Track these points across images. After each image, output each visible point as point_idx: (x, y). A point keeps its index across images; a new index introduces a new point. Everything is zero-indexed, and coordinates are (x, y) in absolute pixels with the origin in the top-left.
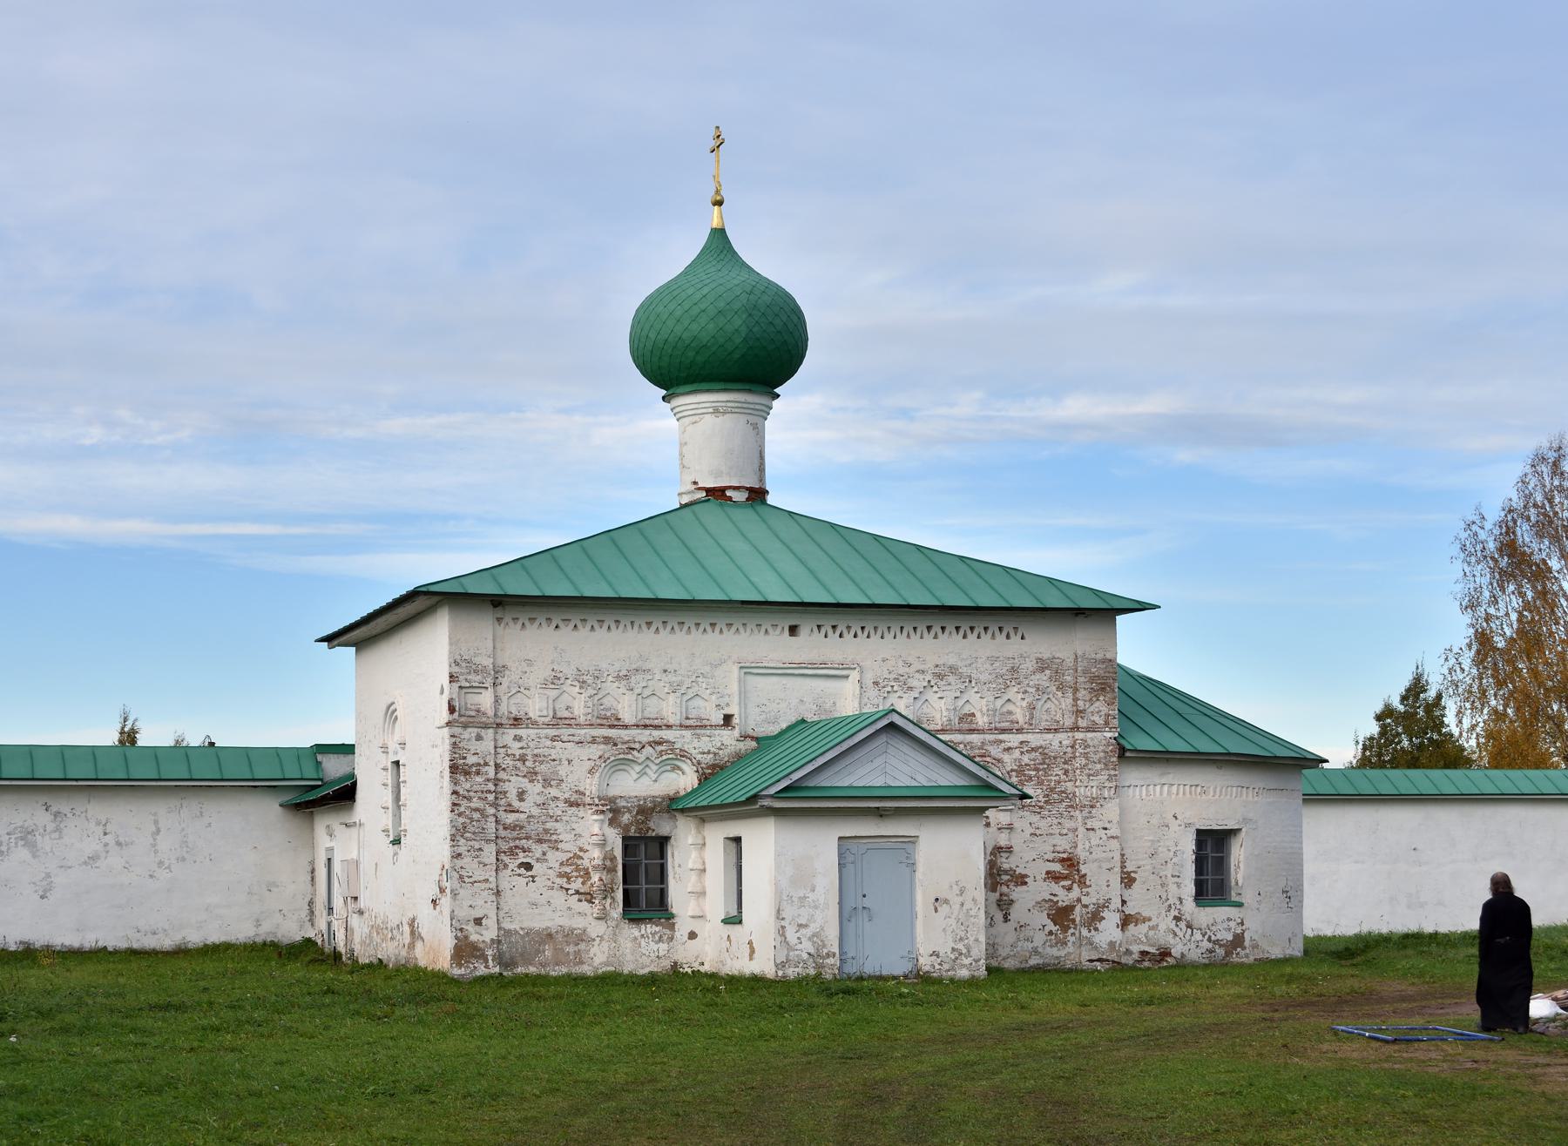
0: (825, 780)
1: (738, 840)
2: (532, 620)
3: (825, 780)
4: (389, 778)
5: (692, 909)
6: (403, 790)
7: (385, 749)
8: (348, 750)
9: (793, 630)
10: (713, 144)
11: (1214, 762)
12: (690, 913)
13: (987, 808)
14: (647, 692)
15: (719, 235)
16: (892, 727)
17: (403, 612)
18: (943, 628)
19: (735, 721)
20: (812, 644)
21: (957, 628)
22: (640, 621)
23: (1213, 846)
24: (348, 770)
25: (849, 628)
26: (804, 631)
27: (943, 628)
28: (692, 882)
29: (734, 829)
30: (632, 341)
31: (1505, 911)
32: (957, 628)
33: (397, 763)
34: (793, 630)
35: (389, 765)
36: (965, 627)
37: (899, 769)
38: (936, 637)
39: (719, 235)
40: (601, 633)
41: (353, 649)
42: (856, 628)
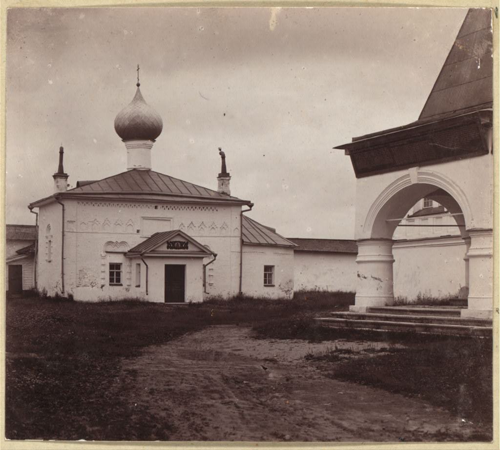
0: (157, 250)
7: (47, 237)
9: (156, 207)
11: (447, 238)
14: (117, 224)
16: (179, 235)
18: (196, 208)
19: (140, 232)
21: (200, 208)
22: (116, 204)
23: (268, 269)
25: (171, 207)
26: (159, 207)
27: (196, 208)
28: (128, 276)
31: (469, 244)
32: (200, 208)
33: (50, 241)
34: (156, 207)
35: (48, 241)
36: (202, 207)
38: (194, 210)
40: (105, 207)
41: (38, 208)
42: (186, 207)
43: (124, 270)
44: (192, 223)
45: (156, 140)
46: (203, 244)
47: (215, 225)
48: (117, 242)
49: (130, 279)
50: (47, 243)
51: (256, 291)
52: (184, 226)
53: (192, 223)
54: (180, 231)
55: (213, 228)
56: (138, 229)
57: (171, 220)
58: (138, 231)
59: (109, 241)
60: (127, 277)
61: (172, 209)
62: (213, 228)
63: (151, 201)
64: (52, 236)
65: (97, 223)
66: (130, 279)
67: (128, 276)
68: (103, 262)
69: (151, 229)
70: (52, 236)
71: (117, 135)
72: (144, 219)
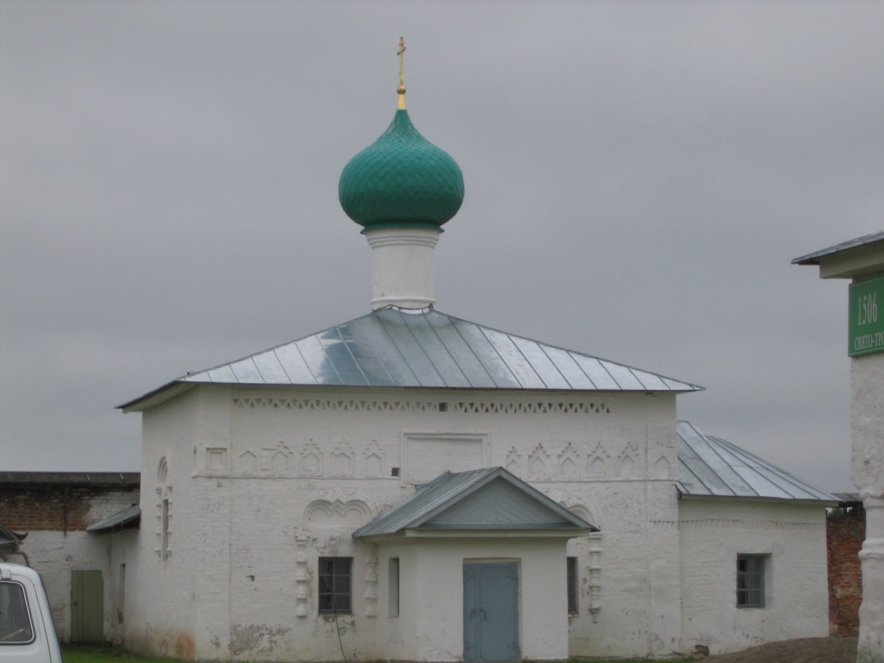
1: (397, 560)
2: (259, 400)
3: (455, 520)
4: (160, 513)
5: (368, 610)
6: (170, 522)
7: (159, 491)
8: (129, 485)
10: (399, 49)
12: (367, 613)
13: (568, 538)
15: (402, 117)
17: (165, 396)
19: (402, 473)
20: (451, 423)
24: (132, 514)
28: (368, 592)
29: (395, 552)
30: (340, 192)
33: (166, 502)
35: (161, 503)
37: (499, 513)
39: (402, 117)
43: (360, 575)
44: (540, 447)
45: (443, 227)
46: (558, 501)
47: (287, 448)
48: (338, 500)
49: (374, 600)
50: (159, 506)
51: (690, 619)
52: (519, 456)
53: (540, 447)
54: (501, 468)
55: (598, 458)
56: (396, 466)
57: (484, 438)
58: (395, 472)
59: (315, 498)
60: (366, 596)
61: (487, 411)
62: (598, 458)
63: (452, 437)
64: (170, 488)
65: (285, 452)
66: (374, 600)
67: (368, 592)
68: (301, 555)
69: (427, 464)
70: (170, 488)
71: (344, 214)
72: (412, 438)
